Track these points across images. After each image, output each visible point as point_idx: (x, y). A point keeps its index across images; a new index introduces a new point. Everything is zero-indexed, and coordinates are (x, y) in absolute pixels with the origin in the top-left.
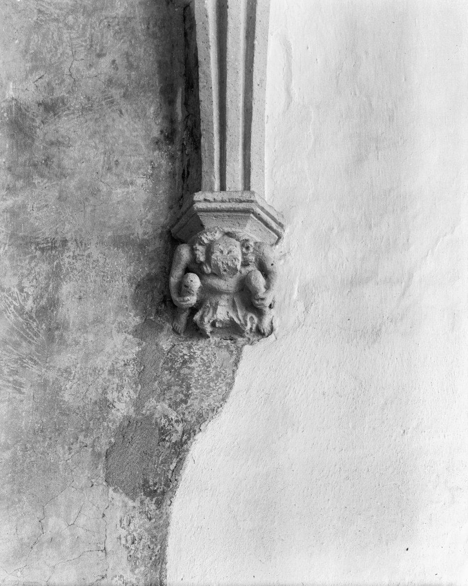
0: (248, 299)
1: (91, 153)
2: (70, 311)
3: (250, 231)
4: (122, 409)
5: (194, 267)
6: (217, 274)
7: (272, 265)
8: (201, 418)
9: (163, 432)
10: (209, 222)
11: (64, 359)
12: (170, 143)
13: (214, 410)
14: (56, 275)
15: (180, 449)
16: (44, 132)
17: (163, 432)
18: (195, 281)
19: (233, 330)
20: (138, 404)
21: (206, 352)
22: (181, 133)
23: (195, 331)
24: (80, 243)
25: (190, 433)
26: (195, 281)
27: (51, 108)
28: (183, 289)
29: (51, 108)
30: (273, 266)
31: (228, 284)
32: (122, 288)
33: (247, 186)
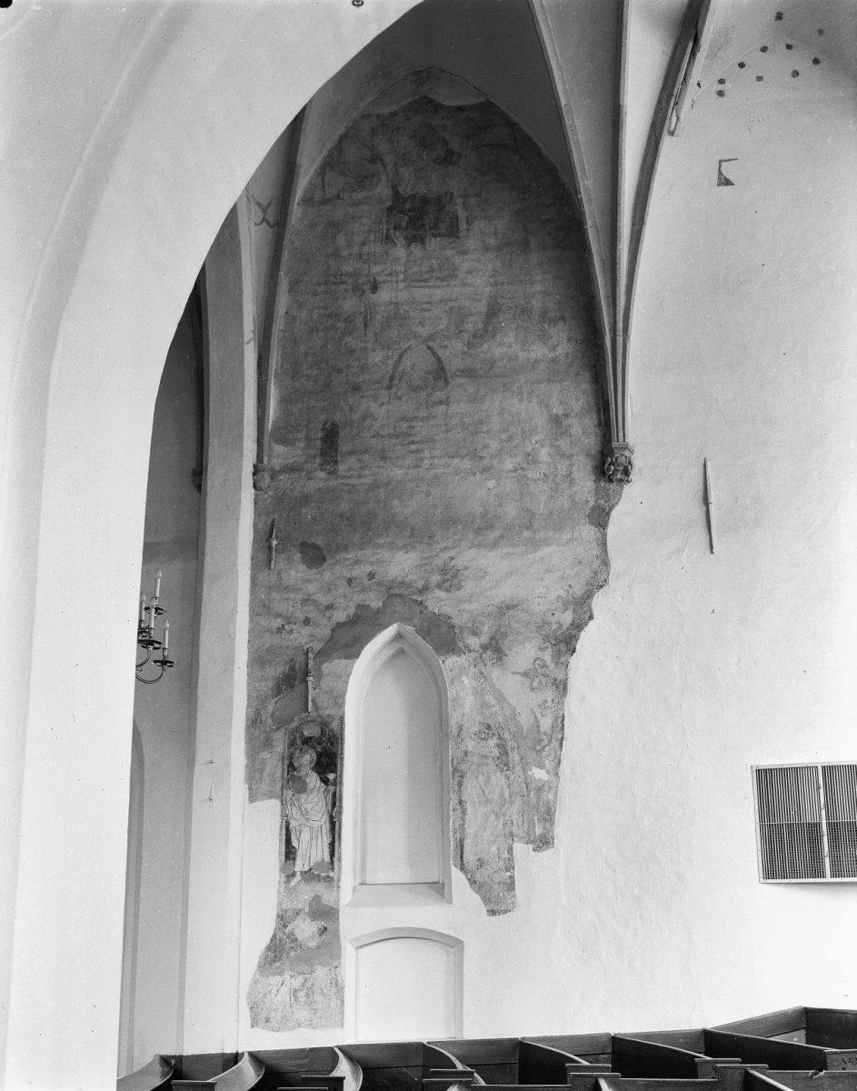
0: (626, 472)
1: (578, 429)
2: (576, 475)
3: (627, 453)
4: (592, 503)
5: (612, 463)
6: (618, 465)
7: (795, 74)
8: (613, 506)
9: (604, 509)
10: (615, 451)
11: (575, 489)
12: (499, 249)
13: (617, 503)
14: (572, 465)
15: (608, 514)
16: (565, 423)
17: (604, 509)
18: (612, 467)
19: (621, 481)
20: (596, 501)
21: (613, 486)
22: (603, 424)
23: (610, 481)
24: (578, 456)
25: (611, 510)
26: (612, 467)
27: (566, 416)
28: (609, 469)
29: (566, 416)
30: (813, 57)
31: (621, 468)
32: (589, 468)
33: (624, 441)
